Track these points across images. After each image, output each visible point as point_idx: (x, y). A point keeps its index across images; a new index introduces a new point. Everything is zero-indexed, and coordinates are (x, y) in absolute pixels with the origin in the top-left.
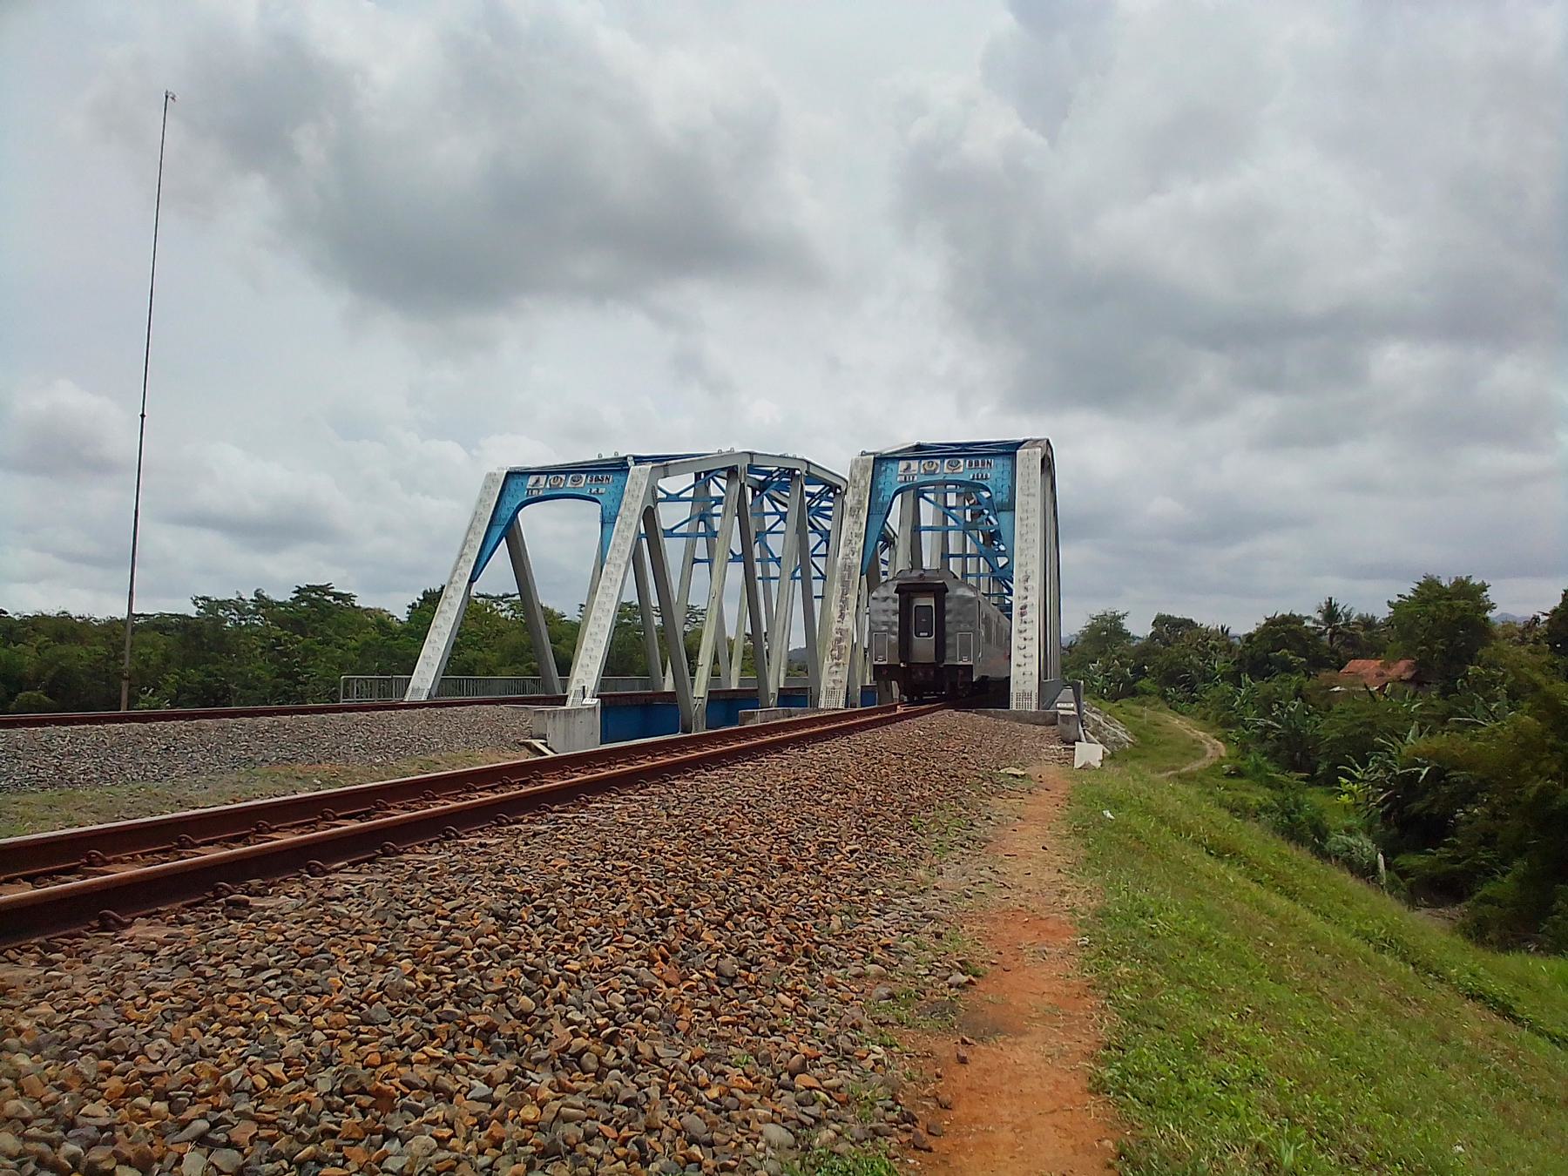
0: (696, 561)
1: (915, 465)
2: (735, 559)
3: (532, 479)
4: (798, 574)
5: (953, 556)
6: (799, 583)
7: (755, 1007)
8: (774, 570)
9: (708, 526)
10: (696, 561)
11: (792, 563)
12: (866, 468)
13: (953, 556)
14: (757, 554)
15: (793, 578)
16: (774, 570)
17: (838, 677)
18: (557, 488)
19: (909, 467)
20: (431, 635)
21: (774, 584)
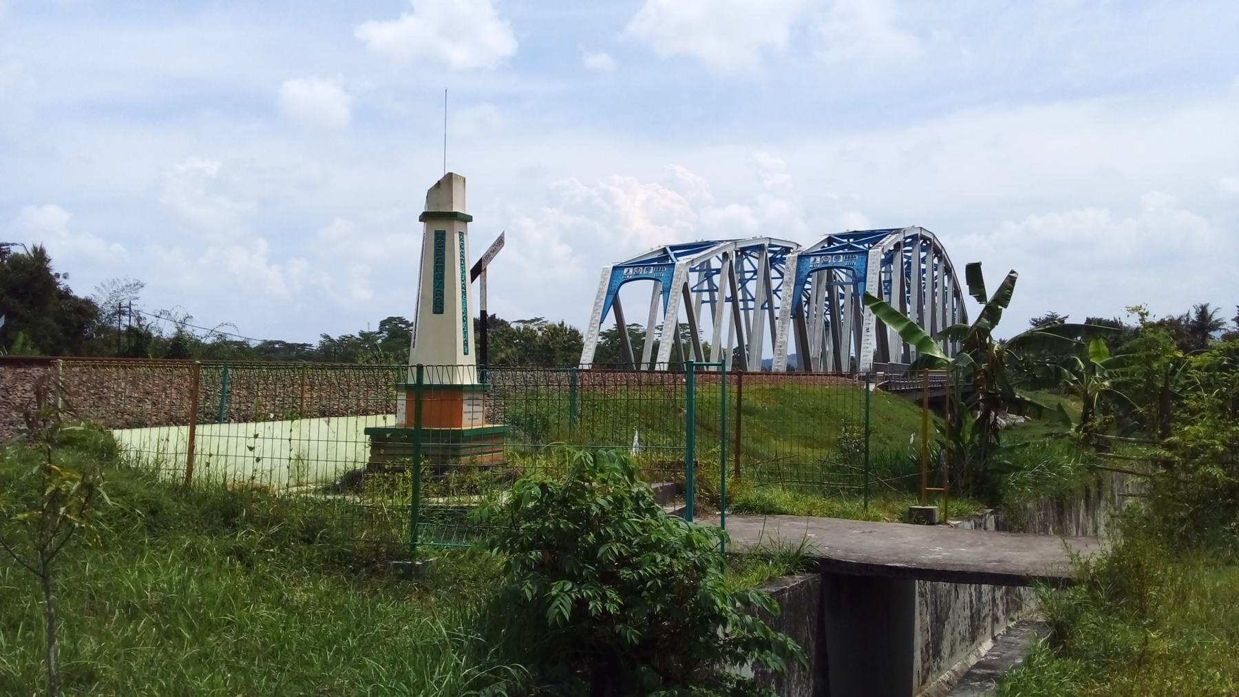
0: (703, 302)
1: (818, 259)
2: (727, 300)
3: (812, 259)
4: (767, 306)
5: (706, 291)
6: (767, 311)
7: (521, 410)
8: (751, 304)
9: (711, 283)
10: (703, 302)
11: (763, 298)
12: (794, 261)
13: (706, 291)
14: (740, 295)
15: (763, 308)
16: (751, 304)
17: (779, 364)
18: (638, 274)
19: (815, 260)
20: (585, 350)
21: (751, 313)
